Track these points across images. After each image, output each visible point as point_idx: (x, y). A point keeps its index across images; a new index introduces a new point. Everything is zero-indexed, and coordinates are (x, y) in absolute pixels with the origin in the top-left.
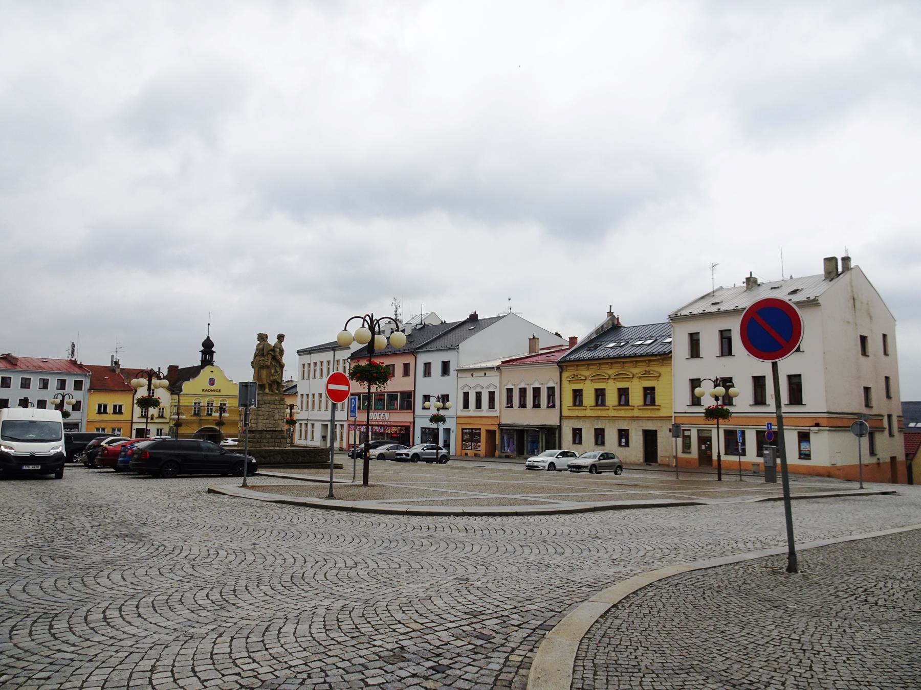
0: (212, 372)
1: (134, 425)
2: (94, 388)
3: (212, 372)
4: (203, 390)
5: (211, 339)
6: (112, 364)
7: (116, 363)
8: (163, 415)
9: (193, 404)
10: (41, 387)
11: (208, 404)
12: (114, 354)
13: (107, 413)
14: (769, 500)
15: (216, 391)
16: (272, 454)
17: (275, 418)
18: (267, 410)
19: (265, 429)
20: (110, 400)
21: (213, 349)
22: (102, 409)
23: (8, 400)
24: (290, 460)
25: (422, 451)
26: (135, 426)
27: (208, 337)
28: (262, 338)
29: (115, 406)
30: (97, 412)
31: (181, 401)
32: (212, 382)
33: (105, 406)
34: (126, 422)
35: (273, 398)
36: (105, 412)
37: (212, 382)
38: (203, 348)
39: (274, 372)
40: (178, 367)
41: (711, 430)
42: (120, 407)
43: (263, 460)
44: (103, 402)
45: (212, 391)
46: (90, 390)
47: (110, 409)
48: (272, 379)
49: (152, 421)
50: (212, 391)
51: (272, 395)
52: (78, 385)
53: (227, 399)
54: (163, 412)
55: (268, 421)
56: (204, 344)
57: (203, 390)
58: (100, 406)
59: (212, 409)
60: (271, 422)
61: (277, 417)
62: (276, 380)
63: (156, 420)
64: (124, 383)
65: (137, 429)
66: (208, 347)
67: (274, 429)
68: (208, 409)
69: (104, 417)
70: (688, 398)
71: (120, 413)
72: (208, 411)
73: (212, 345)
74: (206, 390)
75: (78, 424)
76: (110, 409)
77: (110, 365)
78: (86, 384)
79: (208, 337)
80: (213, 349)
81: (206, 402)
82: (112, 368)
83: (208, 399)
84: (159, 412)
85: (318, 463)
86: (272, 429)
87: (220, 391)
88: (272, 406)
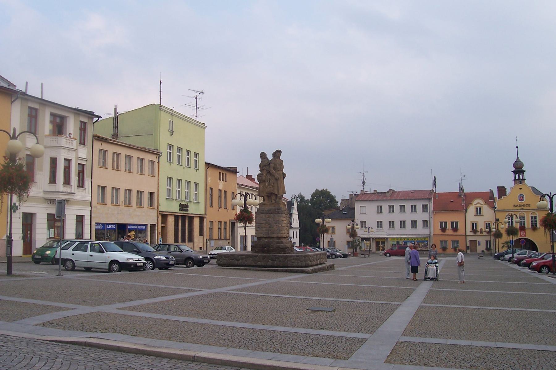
0: (521, 189)
2: (438, 210)
3: (521, 189)
6: (460, 190)
14: (29, 277)
15: (526, 205)
20: (449, 218)
25: (518, 255)
26: (469, 239)
28: (263, 156)
32: (521, 198)
37: (521, 198)
40: (324, 190)
41: (427, 227)
49: (481, 234)
52: (425, 208)
56: (261, 157)
57: (514, 206)
70: (72, 180)
78: (431, 206)
87: (529, 205)
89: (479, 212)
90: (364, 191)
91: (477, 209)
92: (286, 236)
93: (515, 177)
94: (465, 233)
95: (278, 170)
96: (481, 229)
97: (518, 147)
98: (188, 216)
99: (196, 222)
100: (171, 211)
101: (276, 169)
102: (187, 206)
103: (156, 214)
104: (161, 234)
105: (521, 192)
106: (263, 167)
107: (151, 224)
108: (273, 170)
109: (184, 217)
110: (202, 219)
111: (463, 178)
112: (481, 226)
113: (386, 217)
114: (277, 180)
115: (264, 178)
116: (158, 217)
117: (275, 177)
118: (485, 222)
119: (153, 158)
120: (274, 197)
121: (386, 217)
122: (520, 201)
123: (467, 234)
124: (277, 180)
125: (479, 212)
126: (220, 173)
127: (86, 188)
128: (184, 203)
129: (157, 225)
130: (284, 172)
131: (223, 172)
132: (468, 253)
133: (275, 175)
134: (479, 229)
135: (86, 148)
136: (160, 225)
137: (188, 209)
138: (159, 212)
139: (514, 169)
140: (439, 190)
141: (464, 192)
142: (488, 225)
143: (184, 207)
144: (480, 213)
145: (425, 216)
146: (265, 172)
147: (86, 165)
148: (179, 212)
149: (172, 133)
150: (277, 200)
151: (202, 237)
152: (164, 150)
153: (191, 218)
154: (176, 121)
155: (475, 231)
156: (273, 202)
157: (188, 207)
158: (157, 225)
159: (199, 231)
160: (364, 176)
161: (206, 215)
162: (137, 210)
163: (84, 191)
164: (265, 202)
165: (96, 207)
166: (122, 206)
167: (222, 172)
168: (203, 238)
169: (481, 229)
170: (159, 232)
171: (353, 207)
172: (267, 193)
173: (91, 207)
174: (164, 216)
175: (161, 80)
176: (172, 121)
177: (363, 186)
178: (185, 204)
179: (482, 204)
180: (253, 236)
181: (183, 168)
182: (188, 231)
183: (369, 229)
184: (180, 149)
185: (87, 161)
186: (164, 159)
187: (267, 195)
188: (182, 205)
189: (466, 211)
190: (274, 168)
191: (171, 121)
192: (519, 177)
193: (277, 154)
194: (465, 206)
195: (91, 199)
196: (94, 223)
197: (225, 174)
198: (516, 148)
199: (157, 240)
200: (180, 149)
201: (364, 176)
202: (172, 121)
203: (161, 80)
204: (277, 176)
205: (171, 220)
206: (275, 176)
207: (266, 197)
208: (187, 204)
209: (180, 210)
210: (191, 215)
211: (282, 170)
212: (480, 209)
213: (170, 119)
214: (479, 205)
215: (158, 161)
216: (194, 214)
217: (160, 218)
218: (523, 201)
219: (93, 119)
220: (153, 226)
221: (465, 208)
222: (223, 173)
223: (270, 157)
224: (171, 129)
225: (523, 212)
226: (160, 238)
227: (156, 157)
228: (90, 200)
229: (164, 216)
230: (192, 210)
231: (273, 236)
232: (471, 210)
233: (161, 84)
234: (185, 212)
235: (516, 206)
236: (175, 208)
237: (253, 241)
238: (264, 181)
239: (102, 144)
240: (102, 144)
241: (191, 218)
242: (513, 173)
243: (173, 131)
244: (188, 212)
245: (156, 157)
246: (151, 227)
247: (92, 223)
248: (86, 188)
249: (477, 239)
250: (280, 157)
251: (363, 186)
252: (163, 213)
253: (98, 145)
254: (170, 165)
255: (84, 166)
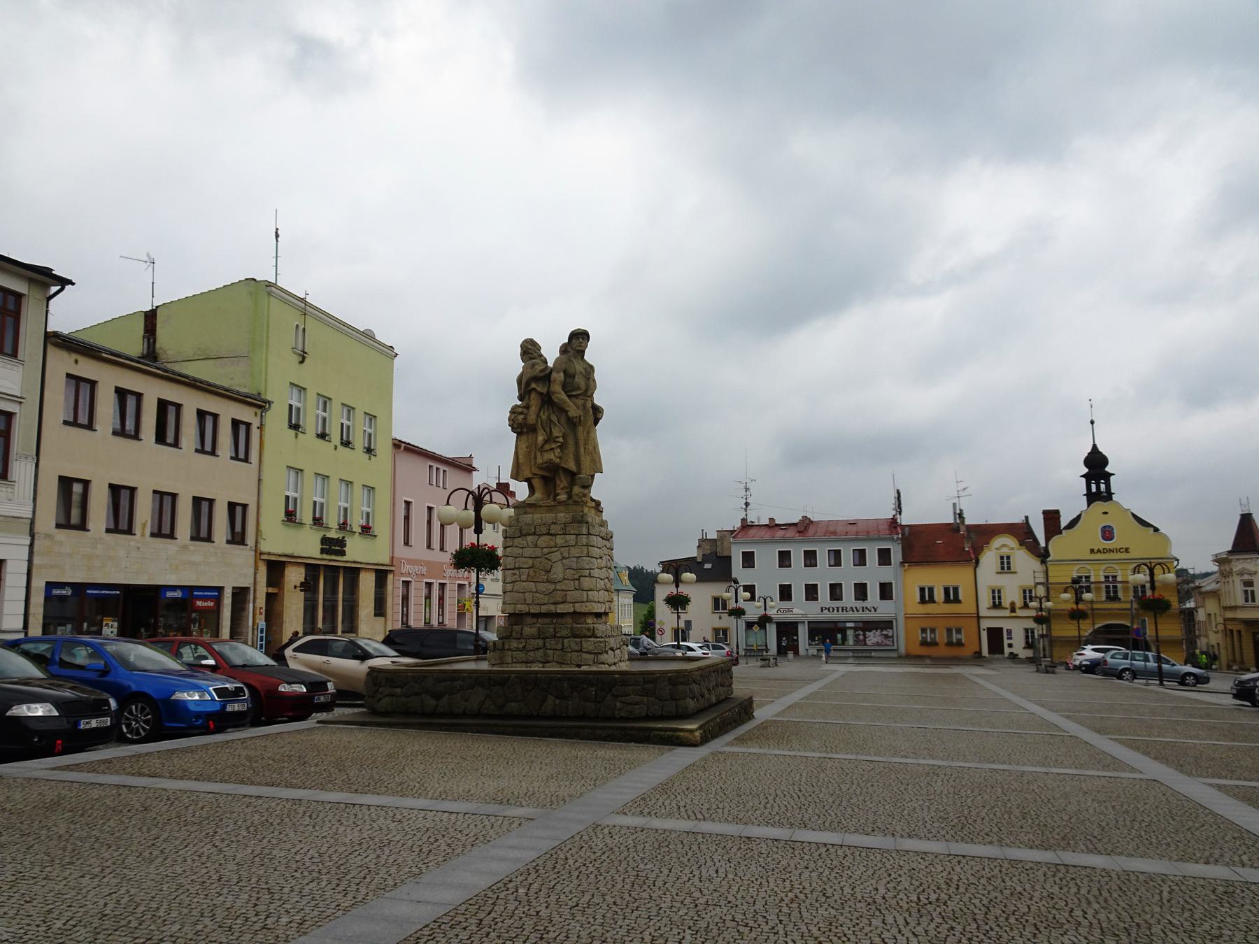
0: (1105, 513)
1: (982, 621)
2: (911, 559)
3: (1105, 513)
4: (1092, 551)
5: (1100, 450)
6: (955, 519)
7: (961, 515)
8: (1000, 603)
9: (1103, 579)
10: (832, 563)
11: (1107, 577)
12: (956, 501)
13: (934, 602)
15: (1119, 550)
16: (458, 684)
17: (552, 576)
18: (528, 552)
19: (524, 608)
20: (938, 578)
21: (1107, 469)
22: (926, 596)
23: (790, 586)
24: (513, 707)
26: (985, 624)
27: (1095, 447)
28: (530, 350)
29: (947, 590)
30: (918, 599)
31: (1050, 574)
32: (1107, 533)
33: (931, 590)
34: (967, 616)
35: (549, 517)
36: (932, 600)
37: (1107, 533)
38: (1086, 470)
39: (546, 442)
42: (956, 589)
43: (433, 702)
44: (926, 584)
45: (1111, 551)
46: (902, 563)
47: (939, 595)
48: (540, 461)
49: (1013, 614)
50: (1111, 551)
51: (550, 508)
52: (884, 557)
53: (1117, 567)
54: (1000, 598)
55: (532, 586)
56: (1087, 462)
57: (1092, 551)
58: (922, 590)
59: (1115, 587)
60: (541, 587)
61: (558, 571)
62: (550, 462)
63: (1019, 613)
64: (964, 548)
65: (988, 629)
66: (1096, 465)
67: (552, 608)
68: (1108, 587)
69: (929, 608)
71: (957, 600)
72: (1108, 592)
73: (1104, 461)
74: (1099, 551)
75: (892, 622)
76: (939, 595)
77: (952, 521)
78: (896, 555)
79: (1095, 447)
80: (1107, 469)
81: (1102, 573)
82: (955, 526)
83: (1104, 567)
84: (994, 598)
85: (612, 718)
86: (544, 609)
87: (1127, 550)
88: (543, 541)
89: (1005, 564)
90: (749, 520)
91: (1002, 558)
92: (603, 611)
93: (1089, 487)
94: (976, 612)
95: (579, 395)
96: (1013, 604)
97: (1095, 420)
98: (344, 567)
99: (367, 583)
100: (295, 555)
101: (572, 391)
102: (341, 543)
103: (252, 561)
104: (264, 613)
105: (1106, 521)
106: (528, 384)
107: (234, 588)
108: (563, 393)
109: (333, 571)
110: (381, 576)
111: (961, 494)
112: (1012, 595)
113: (798, 576)
114: (573, 424)
115: (532, 418)
116: (256, 569)
117: (569, 414)
118: (1020, 587)
119: (246, 414)
120: (563, 482)
121: (798, 576)
122: (1105, 540)
123: (981, 615)
124: (573, 424)
125: (1005, 564)
126: (430, 466)
127: (14, 482)
128: (333, 534)
129: (252, 589)
130: (595, 402)
131: (432, 464)
132: (985, 657)
133: (567, 409)
134: (1006, 603)
135: (21, 366)
136: (262, 590)
137: (344, 551)
138: (258, 553)
139: (1087, 470)
140: (906, 519)
141: (967, 522)
142: (1028, 595)
143: (333, 546)
144: (1009, 568)
145: (887, 574)
146: (535, 401)
147: (18, 415)
148: (319, 556)
149: (304, 358)
150: (576, 490)
151: (381, 619)
152: (280, 398)
153: (353, 573)
154: (311, 324)
155: (997, 605)
156: (563, 497)
157: (345, 546)
158: (252, 589)
159: (373, 605)
160: (747, 489)
161: (392, 566)
162: (192, 548)
163: (9, 490)
164: (538, 495)
165: (48, 536)
166: (143, 535)
167: (435, 465)
168: (383, 623)
169: (1013, 604)
170: (258, 605)
171: (725, 554)
172: (540, 468)
173: (32, 536)
174: (276, 569)
175: (277, 229)
176: (304, 329)
177: (746, 510)
178: (336, 537)
179: (1013, 549)
180: (158, 496)
181: (333, 447)
182: (343, 605)
183: (765, 600)
184: (326, 401)
185: (21, 403)
186: (276, 418)
187: (541, 473)
188: (329, 539)
189: (977, 562)
190: (564, 387)
191: (301, 327)
192: (1098, 487)
193: (579, 339)
194: (971, 551)
195: (34, 512)
196: (39, 584)
197: (444, 471)
198: (1090, 425)
199: (250, 629)
200: (326, 401)
201: (747, 489)
202: (304, 329)
203: (277, 229)
204: (573, 412)
205: (294, 576)
206: (567, 412)
207: (536, 482)
208: (344, 537)
209: (323, 551)
210: (353, 565)
211: (589, 394)
212: (1008, 558)
213: (297, 323)
214: (1005, 551)
215: (261, 425)
216: (361, 563)
217: (263, 570)
218: (1111, 540)
219: (47, 286)
220: (240, 595)
221: (973, 556)
222: (437, 469)
223: (551, 354)
224: (300, 348)
225: (1112, 565)
226: (262, 623)
227: (256, 414)
228: (31, 516)
229: (276, 569)
230: (357, 551)
231: (561, 609)
232: (989, 559)
233: (279, 239)
234: (334, 557)
235: (1095, 551)
236: (307, 544)
237: (459, 636)
238: (533, 429)
239: (76, 362)
240: (76, 362)
241: (353, 573)
242: (1084, 479)
243: (306, 351)
244: (344, 558)
245: (256, 414)
246: (233, 593)
247: (34, 583)
248: (14, 482)
249: (1005, 625)
250: (584, 351)
251: (746, 510)
252: (273, 558)
253: (61, 363)
254: (296, 437)
255: (13, 421)
